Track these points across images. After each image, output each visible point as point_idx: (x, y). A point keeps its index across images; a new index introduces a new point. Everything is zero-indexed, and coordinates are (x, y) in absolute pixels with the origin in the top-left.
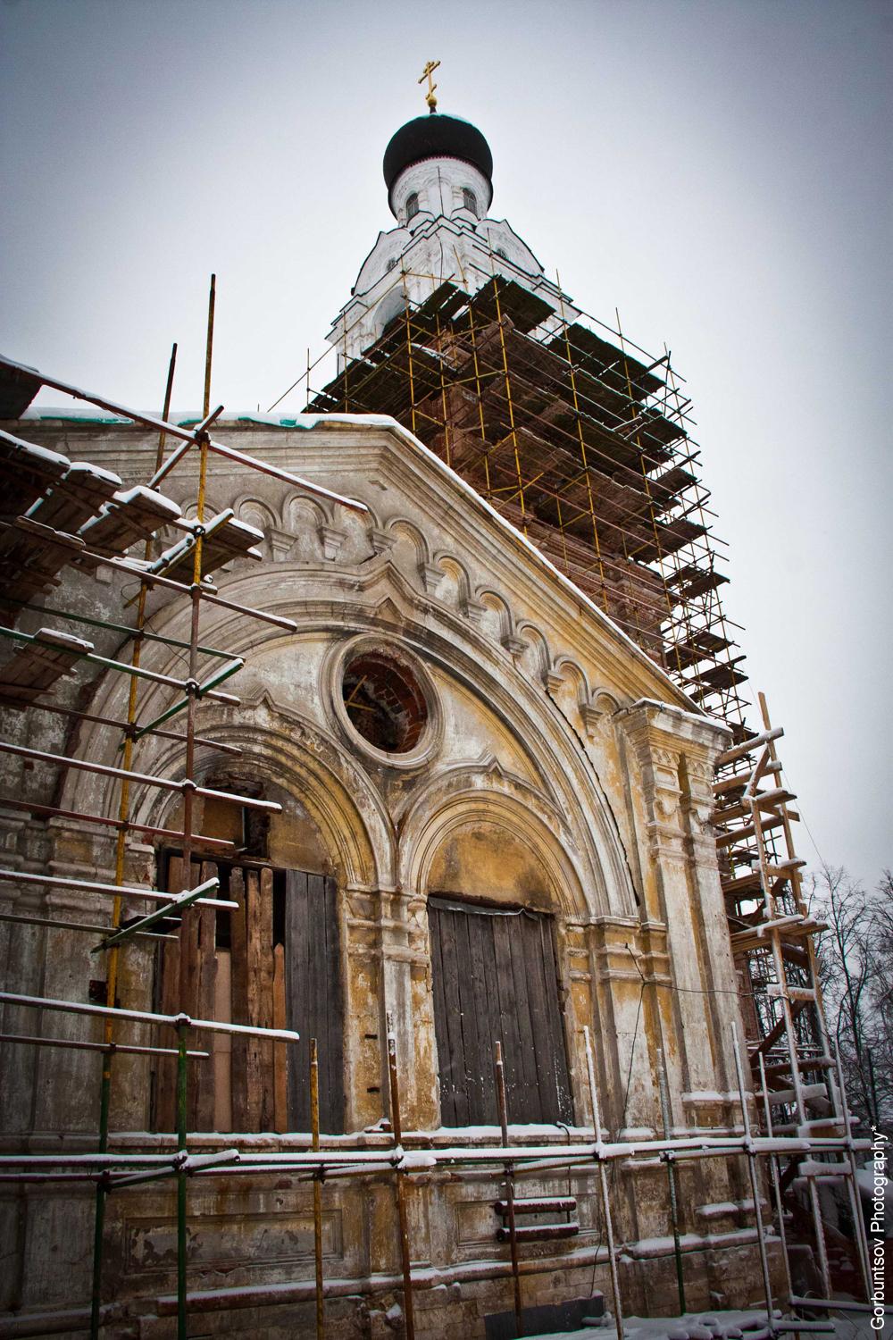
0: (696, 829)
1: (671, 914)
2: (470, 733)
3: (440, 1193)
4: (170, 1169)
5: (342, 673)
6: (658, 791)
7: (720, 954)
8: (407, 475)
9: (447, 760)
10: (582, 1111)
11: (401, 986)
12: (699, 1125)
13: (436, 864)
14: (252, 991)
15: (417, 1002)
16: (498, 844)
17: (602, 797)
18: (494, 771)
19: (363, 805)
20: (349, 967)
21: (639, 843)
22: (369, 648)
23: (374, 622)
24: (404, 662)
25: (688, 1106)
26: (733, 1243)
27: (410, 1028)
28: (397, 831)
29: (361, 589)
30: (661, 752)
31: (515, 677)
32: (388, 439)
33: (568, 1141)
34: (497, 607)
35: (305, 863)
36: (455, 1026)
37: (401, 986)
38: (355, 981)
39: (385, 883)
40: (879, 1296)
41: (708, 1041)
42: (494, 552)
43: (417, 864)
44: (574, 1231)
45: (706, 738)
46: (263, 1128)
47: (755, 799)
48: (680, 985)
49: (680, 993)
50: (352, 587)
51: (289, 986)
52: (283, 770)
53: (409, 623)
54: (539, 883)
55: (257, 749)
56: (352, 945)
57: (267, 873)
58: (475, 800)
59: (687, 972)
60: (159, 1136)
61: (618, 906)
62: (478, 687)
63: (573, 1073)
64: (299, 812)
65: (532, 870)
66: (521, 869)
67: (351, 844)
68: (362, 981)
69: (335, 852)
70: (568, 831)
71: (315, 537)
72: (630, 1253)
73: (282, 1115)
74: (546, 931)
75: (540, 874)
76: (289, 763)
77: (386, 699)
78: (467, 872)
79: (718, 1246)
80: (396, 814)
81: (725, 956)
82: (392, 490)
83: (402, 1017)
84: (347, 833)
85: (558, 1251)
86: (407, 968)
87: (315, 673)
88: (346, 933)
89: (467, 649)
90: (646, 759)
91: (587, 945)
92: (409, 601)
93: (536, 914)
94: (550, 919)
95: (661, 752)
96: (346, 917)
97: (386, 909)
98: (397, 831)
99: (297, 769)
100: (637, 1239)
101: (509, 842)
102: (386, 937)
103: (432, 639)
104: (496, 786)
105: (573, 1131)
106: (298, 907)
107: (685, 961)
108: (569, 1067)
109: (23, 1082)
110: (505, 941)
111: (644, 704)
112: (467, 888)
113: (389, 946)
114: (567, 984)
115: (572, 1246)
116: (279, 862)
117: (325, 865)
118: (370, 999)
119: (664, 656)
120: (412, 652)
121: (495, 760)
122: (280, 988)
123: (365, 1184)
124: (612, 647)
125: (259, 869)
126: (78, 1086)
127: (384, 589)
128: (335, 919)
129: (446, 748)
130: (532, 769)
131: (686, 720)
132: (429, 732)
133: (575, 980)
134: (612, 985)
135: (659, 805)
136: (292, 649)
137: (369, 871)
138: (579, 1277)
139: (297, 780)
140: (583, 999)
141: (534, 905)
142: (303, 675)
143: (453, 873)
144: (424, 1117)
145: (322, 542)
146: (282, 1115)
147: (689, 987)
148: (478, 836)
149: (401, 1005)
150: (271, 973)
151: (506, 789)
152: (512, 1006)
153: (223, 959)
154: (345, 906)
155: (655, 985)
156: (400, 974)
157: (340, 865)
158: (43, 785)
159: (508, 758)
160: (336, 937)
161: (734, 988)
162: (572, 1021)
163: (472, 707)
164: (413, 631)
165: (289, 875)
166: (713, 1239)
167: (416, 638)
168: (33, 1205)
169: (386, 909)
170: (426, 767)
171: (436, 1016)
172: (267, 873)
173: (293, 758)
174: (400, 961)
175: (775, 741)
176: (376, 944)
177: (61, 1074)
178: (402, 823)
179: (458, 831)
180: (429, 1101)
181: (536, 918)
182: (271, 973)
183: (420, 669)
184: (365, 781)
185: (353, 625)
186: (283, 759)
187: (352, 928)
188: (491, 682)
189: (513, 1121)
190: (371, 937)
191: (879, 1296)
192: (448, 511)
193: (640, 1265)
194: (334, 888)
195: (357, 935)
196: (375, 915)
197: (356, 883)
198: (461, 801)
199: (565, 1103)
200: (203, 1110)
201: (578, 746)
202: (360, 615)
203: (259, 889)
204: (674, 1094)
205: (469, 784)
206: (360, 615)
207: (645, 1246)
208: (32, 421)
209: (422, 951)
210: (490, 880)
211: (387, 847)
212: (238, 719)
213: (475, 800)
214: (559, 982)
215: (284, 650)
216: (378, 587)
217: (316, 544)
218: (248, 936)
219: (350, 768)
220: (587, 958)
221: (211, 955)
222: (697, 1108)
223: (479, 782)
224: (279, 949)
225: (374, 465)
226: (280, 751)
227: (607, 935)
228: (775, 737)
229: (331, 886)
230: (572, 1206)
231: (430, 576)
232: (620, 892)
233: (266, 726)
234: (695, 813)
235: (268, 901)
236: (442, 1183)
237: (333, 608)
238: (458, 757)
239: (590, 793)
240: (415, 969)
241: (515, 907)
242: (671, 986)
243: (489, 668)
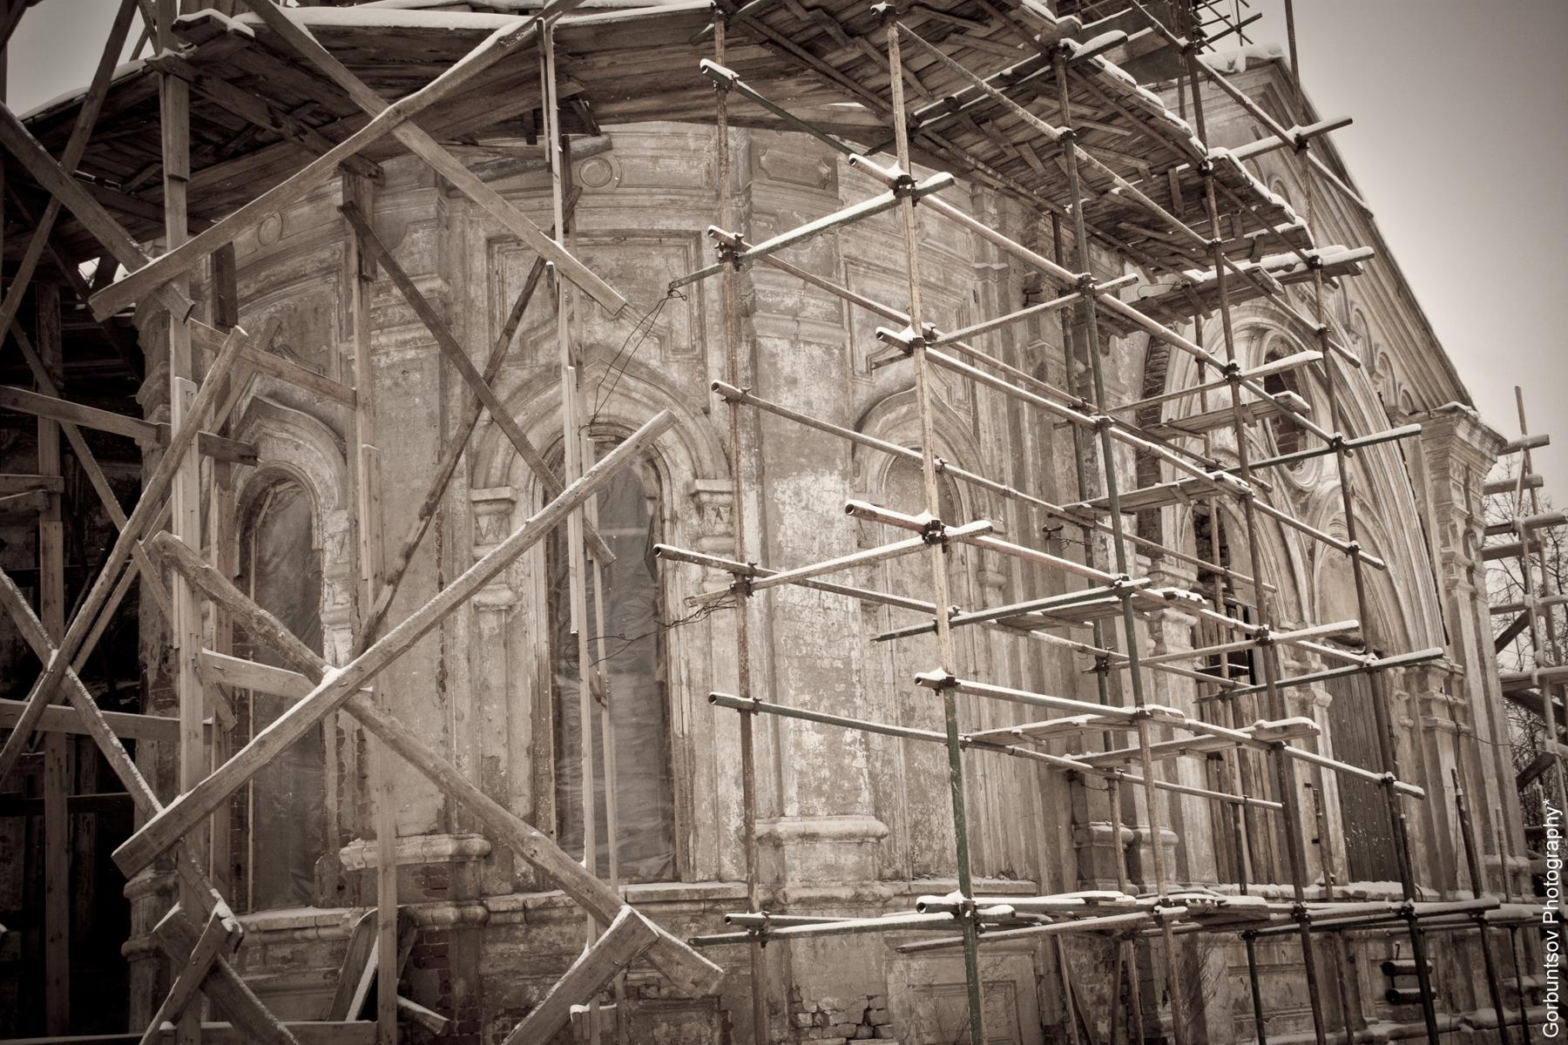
4: (947, 916)
40: (1552, 997)
42: (1338, 216)
72: (1468, 1022)
90: (1442, 472)
111: (1455, 409)
119: (1175, 187)
133: (1403, 726)
134: (1437, 734)
144: (837, 669)
175: (1532, 451)
191: (1552, 997)
193: (1483, 1036)
220: (1408, 702)
228: (1535, 445)
232: (1433, 630)
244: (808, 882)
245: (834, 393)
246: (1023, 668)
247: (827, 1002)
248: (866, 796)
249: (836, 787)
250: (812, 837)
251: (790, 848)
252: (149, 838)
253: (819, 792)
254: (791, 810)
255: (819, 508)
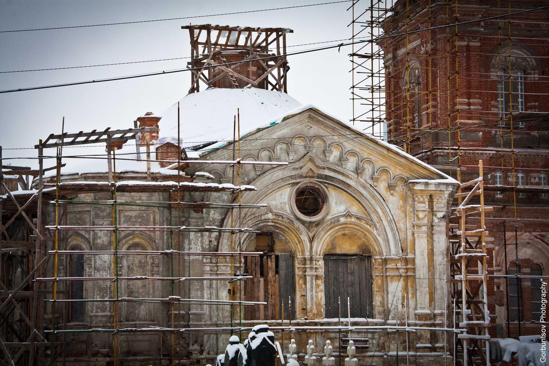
0: (436, 220)
1: (417, 253)
2: (341, 203)
3: (322, 335)
5: (295, 196)
6: (417, 211)
7: (440, 264)
8: (318, 121)
9: (331, 214)
10: (376, 314)
11: (312, 282)
12: (419, 320)
13: (328, 245)
14: (269, 287)
15: (318, 286)
16: (351, 237)
17: (391, 217)
18: (348, 215)
19: (301, 234)
20: (297, 278)
21: (408, 229)
22: (304, 186)
23: (306, 177)
24: (317, 187)
25: (416, 315)
26: (428, 356)
27: (314, 293)
28: (311, 240)
29: (301, 168)
30: (419, 197)
31: (358, 182)
32: (310, 111)
33: (367, 324)
34: (354, 156)
35: (285, 252)
36: (331, 291)
37: (312, 282)
38: (299, 282)
39: (307, 255)
40: (544, 348)
41: (428, 294)
43: (320, 247)
44: (368, 348)
45: (443, 188)
46: (272, 319)
47: (464, 208)
48: (417, 276)
49: (417, 280)
50: (298, 168)
51: (279, 284)
52: (277, 228)
53: (318, 174)
54: (366, 246)
55: (270, 224)
56: (298, 272)
57: (273, 257)
58: (342, 224)
59: (422, 271)
60: (246, 321)
61: (394, 251)
62: (344, 187)
63: (374, 303)
64: (283, 238)
65: (364, 242)
66: (360, 242)
67: (298, 245)
68: (301, 282)
69: (294, 248)
70: (377, 229)
71: (286, 154)
72: (387, 355)
73: (277, 316)
74: (368, 261)
75: (367, 243)
76: (279, 226)
77: (310, 201)
78: (339, 246)
79: (420, 356)
80: (311, 235)
81: (443, 265)
82: (314, 127)
83: (312, 290)
84: (297, 242)
85: (362, 352)
86: (314, 278)
87: (287, 198)
88: (297, 269)
89: (340, 177)
91: (382, 265)
92: (318, 167)
93: (365, 256)
94: (370, 257)
95: (419, 197)
96: (297, 265)
97: (308, 262)
98: (311, 240)
99: (282, 227)
100: (389, 351)
101: (355, 235)
102: (308, 270)
103: (327, 177)
104: (349, 219)
105: (370, 320)
106: (282, 264)
107: (422, 268)
108: (372, 302)
109: (215, 311)
110: (352, 266)
112: (338, 251)
113: (308, 272)
114: (374, 277)
115: (367, 352)
116: (277, 253)
117: (291, 251)
118: (303, 286)
120: (319, 183)
121: (349, 212)
122: (277, 285)
123: (299, 332)
124: (403, 160)
125: (271, 256)
126: (227, 311)
127: (310, 165)
128: (293, 266)
129: (331, 211)
130: (364, 210)
131: (431, 184)
132: (325, 207)
133: (376, 276)
135: (417, 216)
136: (280, 192)
137: (303, 252)
138: (367, 359)
139: (282, 230)
140: (380, 282)
141: (363, 253)
142: (283, 201)
143: (333, 246)
145: (288, 155)
146: (277, 316)
147: (422, 277)
148: (344, 235)
149: (312, 287)
150: (275, 282)
151: (353, 220)
152: (352, 285)
153: (262, 280)
154: (296, 262)
155: (409, 278)
156: (312, 279)
157: (295, 251)
158: (214, 245)
159: (355, 209)
160: (293, 271)
161: (445, 277)
162: (375, 288)
163: (343, 194)
164: (319, 176)
165: (280, 257)
166: (418, 354)
167: (321, 178)
168: (219, 335)
169: (308, 262)
170: (323, 219)
171: (325, 289)
172: (273, 257)
173: (280, 224)
174: (312, 276)
176: (305, 271)
177: (223, 309)
178: (313, 238)
179: (336, 234)
180: (321, 312)
181: (364, 258)
182: (275, 282)
183: (322, 188)
184: (302, 227)
185: (298, 180)
186: (277, 225)
187: (298, 268)
188: (349, 186)
189: (342, 317)
190: (304, 270)
191: (544, 348)
192: (334, 129)
194: (293, 257)
195: (300, 269)
196: (305, 264)
197: (299, 256)
198: (336, 226)
199: (370, 312)
200: (257, 315)
201: (382, 201)
202: (301, 176)
203: (271, 261)
204: (411, 310)
205: (338, 221)
206: (301, 176)
207: (391, 353)
208: (232, 358)
209: (321, 272)
210: (347, 247)
211: (309, 245)
212: (263, 218)
213: (342, 224)
214: (371, 276)
215: (276, 194)
216: (307, 165)
217: (287, 156)
218: (268, 273)
219: (297, 224)
221: (258, 279)
222: (419, 315)
223: (342, 220)
224: (277, 276)
225: (307, 120)
226: (277, 223)
227: (388, 262)
229: (292, 256)
230: (367, 341)
231: (327, 154)
233: (271, 218)
234: (436, 215)
235: (274, 264)
236: (322, 333)
237: (291, 177)
238: (336, 212)
239: (386, 216)
240: (317, 277)
241: (356, 255)
242: (414, 277)
243: (348, 181)
244: (96, 323)
245: (109, 238)
246: (375, 244)
247: (98, 343)
248: (108, 309)
249: (103, 307)
250: (97, 316)
251: (94, 318)
252: (173, 326)
253: (99, 308)
254: (94, 311)
255: (104, 260)
